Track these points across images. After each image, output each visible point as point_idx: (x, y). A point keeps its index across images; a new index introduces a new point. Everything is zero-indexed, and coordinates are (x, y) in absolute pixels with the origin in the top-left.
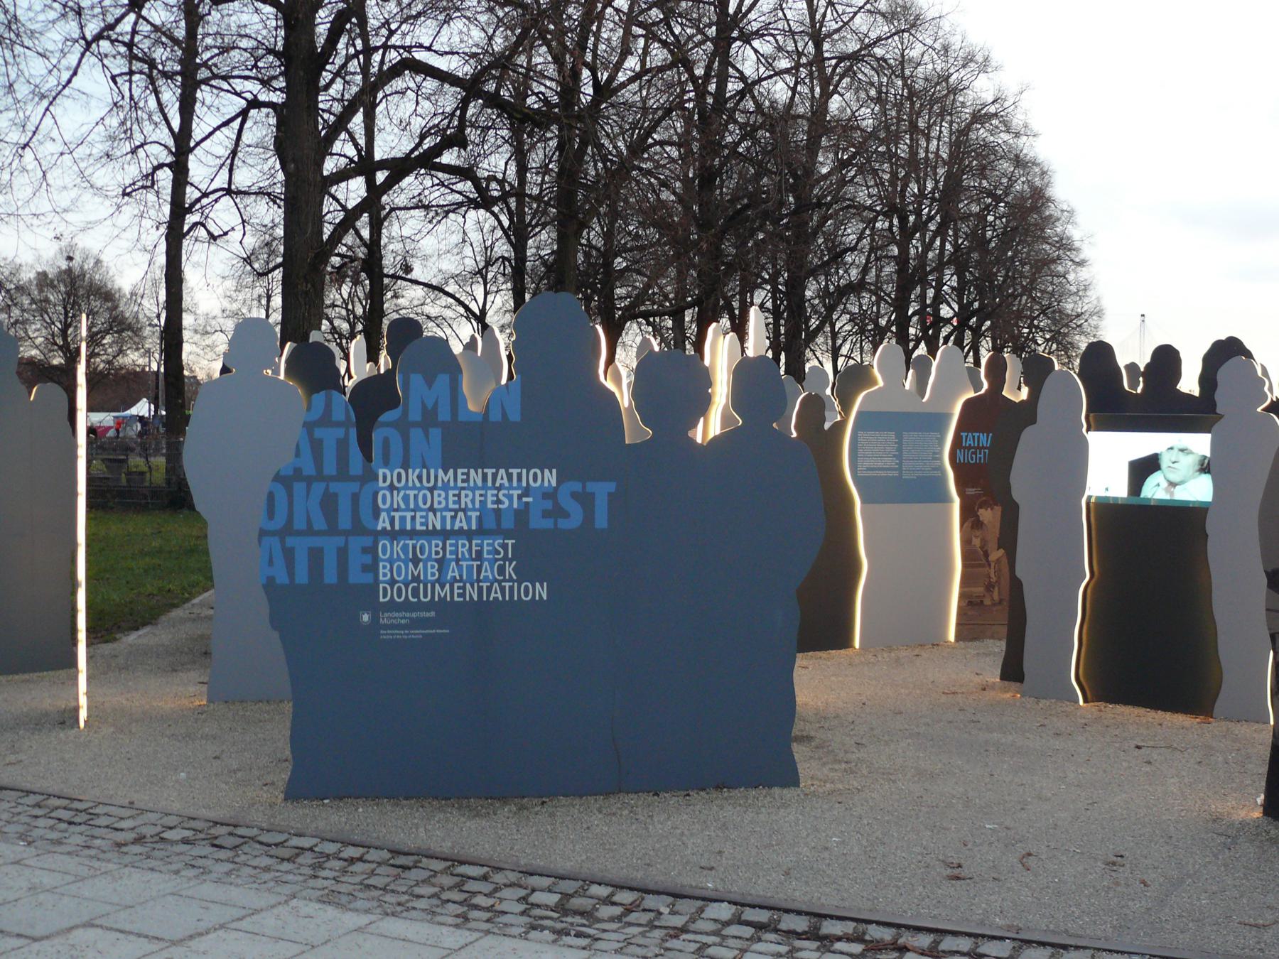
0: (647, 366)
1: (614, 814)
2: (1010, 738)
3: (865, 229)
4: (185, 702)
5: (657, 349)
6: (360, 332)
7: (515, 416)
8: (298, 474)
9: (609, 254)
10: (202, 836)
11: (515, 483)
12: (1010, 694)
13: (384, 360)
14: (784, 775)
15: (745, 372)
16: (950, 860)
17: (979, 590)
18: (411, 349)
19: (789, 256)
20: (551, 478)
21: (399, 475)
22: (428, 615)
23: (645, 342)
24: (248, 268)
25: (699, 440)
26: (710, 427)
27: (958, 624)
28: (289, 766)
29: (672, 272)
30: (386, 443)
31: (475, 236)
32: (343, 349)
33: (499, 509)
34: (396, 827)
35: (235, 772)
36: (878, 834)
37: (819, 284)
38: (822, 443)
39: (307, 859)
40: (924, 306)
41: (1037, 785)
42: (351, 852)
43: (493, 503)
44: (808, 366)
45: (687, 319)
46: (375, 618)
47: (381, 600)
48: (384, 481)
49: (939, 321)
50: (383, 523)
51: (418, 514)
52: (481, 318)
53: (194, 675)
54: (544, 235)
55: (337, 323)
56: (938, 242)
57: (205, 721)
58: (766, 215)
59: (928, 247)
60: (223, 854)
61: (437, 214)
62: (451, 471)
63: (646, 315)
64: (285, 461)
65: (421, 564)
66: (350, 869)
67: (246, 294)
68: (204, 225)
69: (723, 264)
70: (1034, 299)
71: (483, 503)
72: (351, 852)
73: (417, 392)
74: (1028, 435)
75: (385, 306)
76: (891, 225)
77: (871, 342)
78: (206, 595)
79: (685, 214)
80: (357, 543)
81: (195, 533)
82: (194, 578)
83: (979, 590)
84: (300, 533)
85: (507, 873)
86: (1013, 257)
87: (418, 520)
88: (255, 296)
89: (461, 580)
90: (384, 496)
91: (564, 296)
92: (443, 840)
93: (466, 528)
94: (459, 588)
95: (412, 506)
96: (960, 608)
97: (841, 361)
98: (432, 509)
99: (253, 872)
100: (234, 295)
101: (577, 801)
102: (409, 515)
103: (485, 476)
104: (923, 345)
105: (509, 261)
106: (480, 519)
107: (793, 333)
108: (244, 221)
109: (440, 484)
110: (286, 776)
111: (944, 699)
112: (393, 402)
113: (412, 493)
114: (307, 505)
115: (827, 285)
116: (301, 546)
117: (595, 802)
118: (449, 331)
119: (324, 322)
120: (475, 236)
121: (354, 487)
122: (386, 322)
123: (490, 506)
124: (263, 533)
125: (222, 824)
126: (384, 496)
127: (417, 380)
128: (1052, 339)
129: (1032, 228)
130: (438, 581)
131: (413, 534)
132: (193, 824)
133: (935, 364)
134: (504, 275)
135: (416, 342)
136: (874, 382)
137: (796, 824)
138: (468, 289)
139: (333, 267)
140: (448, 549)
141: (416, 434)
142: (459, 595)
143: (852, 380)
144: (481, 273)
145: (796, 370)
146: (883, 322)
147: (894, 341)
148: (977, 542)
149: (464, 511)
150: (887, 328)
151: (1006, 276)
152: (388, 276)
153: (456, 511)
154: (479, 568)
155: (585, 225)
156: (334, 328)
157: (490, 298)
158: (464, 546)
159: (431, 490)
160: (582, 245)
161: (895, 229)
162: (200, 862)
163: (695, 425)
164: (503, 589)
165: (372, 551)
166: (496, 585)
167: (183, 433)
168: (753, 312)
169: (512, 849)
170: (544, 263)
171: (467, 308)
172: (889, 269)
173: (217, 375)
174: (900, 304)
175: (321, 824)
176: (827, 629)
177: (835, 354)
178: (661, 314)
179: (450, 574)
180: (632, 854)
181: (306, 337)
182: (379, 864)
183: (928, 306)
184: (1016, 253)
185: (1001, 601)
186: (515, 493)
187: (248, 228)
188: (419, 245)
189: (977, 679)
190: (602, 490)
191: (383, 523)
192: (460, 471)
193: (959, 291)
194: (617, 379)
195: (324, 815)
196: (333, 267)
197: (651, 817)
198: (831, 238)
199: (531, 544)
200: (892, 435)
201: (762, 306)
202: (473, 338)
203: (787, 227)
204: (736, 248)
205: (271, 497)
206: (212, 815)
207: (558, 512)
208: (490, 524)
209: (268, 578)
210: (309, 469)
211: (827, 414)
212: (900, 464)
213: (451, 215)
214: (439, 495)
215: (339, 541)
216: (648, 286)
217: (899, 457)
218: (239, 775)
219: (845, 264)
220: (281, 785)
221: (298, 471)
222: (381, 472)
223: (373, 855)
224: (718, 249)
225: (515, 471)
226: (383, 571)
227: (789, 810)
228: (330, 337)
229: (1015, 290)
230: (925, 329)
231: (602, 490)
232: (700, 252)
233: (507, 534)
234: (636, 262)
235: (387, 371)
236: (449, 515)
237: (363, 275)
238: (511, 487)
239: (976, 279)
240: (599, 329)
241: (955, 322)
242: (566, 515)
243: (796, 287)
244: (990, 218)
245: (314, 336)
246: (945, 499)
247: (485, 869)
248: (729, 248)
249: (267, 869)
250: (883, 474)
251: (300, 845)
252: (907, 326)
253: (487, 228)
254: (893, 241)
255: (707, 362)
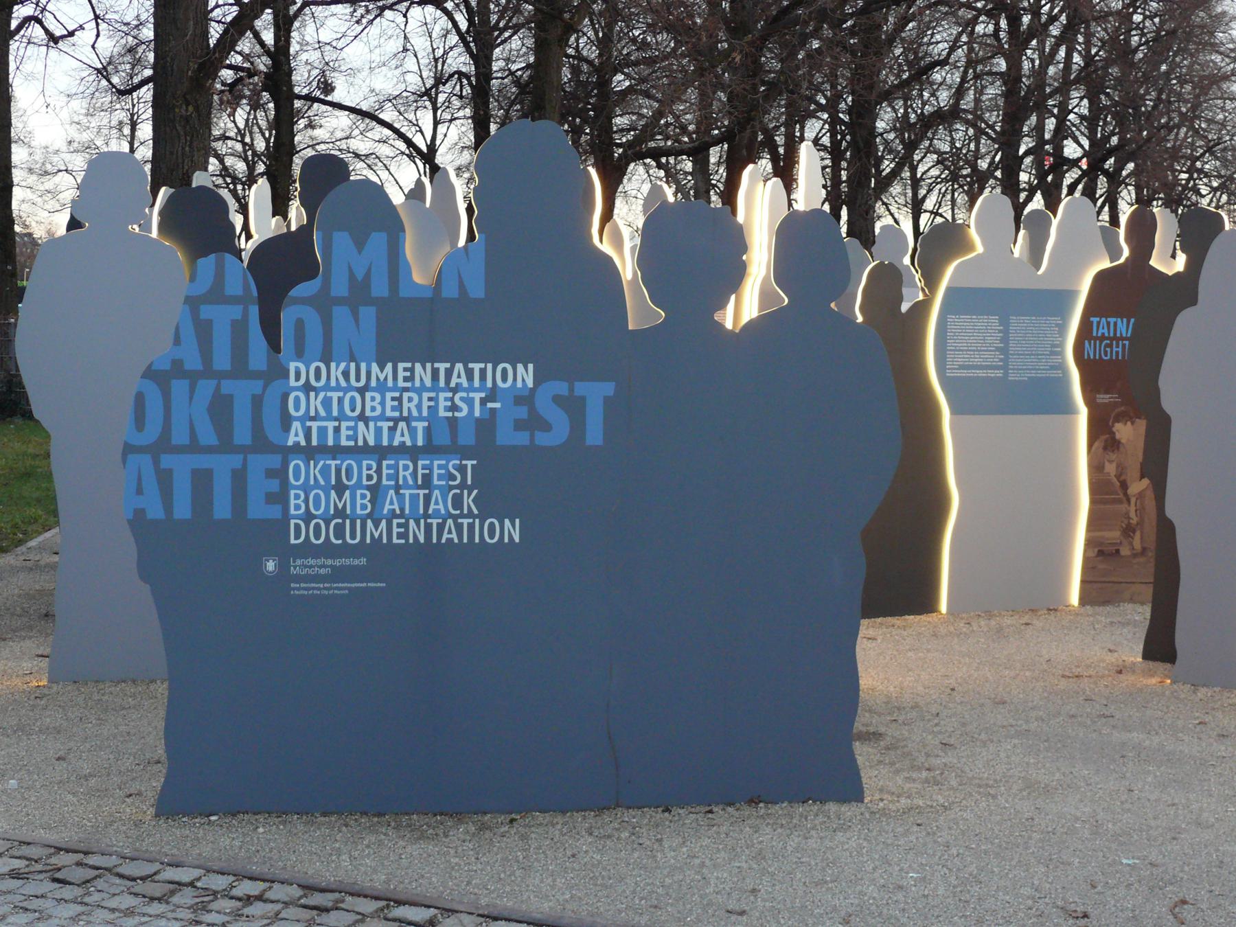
0: (658, 222)
1: (609, 837)
2: (1156, 740)
3: (960, 34)
4: (17, 682)
5: (671, 199)
6: (262, 174)
7: (477, 290)
8: (178, 369)
9: (605, 70)
10: (39, 867)
11: (477, 383)
12: (1156, 679)
13: (296, 213)
14: (845, 787)
15: (793, 232)
16: (1073, 907)
17: (1114, 535)
18: (336, 196)
19: (855, 73)
20: (525, 375)
21: (318, 370)
22: (356, 562)
23: (655, 191)
24: (104, 83)
25: (729, 325)
26: (744, 307)
27: (1084, 582)
28: (162, 769)
29: (692, 94)
30: (300, 325)
31: (420, 43)
32: (238, 199)
33: (455, 419)
34: (311, 853)
35: (86, 778)
36: (973, 868)
37: (895, 111)
38: (897, 330)
39: (185, 898)
40: (1041, 142)
41: (1195, 806)
42: (247, 888)
43: (448, 409)
44: (878, 226)
45: (713, 160)
46: (283, 566)
47: (293, 541)
48: (298, 378)
49: (1062, 163)
50: (296, 436)
51: (344, 425)
52: (429, 156)
53: (31, 645)
54: (515, 43)
55: (229, 161)
56: (1062, 53)
57: (45, 708)
58: (823, 16)
59: (1048, 60)
60: (68, 892)
61: (368, 11)
62: (389, 365)
63: (656, 154)
64: (160, 351)
65: (347, 493)
66: (246, 911)
67: (102, 119)
68: (40, 22)
69: (763, 83)
70: (1196, 132)
71: (433, 410)
72: (247, 888)
73: (341, 256)
74: (1185, 320)
75: (296, 139)
76: (997, 29)
77: (967, 193)
78: (48, 535)
79: (711, 14)
80: (259, 463)
81: (31, 451)
82: (32, 511)
83: (1114, 535)
84: (178, 450)
85: (463, 916)
86: (1167, 73)
87: (344, 433)
88: (114, 123)
89: (402, 515)
90: (297, 399)
91: (547, 127)
92: (375, 871)
93: (409, 443)
94: (399, 525)
95: (335, 413)
96: (1087, 561)
97: (924, 219)
98: (362, 417)
99: (110, 916)
100: (84, 120)
101: (559, 819)
102: (331, 425)
103: (435, 373)
104: (1038, 196)
105: (468, 77)
106: (428, 431)
107: (859, 180)
108: (97, 17)
109: (373, 383)
110: (158, 784)
111: (1063, 684)
112: (310, 270)
113: (335, 396)
114: (191, 410)
115: (906, 114)
116: (182, 467)
117: (582, 821)
118: (384, 175)
119: (212, 160)
120: (420, 43)
121: (256, 386)
122: (298, 162)
123: (442, 413)
124: (128, 449)
125: (68, 851)
126: (297, 399)
127: (342, 240)
128: (1222, 188)
129: (1197, 31)
130: (370, 516)
132: (25, 851)
133: (1055, 222)
134: (461, 97)
135: (342, 188)
136: (970, 247)
137: (860, 854)
138: (411, 117)
139: (223, 84)
140: (385, 472)
141: (341, 314)
142: (400, 536)
143: (940, 244)
144: (429, 94)
145: (862, 231)
146: (983, 165)
147: (999, 190)
148: (1111, 469)
149: (407, 420)
150: (989, 173)
151: (1158, 100)
152: (299, 97)
153: (396, 421)
154: (427, 499)
155: (572, 28)
156: (225, 168)
157: (442, 129)
158: (406, 468)
159: (362, 391)
160: (568, 56)
161: (1002, 34)
162: (35, 904)
163: (722, 305)
164: (459, 528)
165: (280, 474)
166: (450, 521)
167: (16, 312)
168: (806, 152)
169: (469, 883)
170: (517, 82)
171: (409, 143)
172: (993, 90)
173: (62, 231)
174: (1008, 140)
175: (206, 850)
176: (900, 584)
177: (917, 208)
178: (677, 153)
179: (387, 507)
180: (634, 892)
181: (188, 182)
182: (286, 904)
183: (1047, 142)
184: (1173, 66)
185: (1144, 550)
186: (477, 396)
187: (103, 26)
188: (343, 54)
189: (1111, 658)
190: (596, 393)
191: (296, 436)
192: (401, 366)
193: (1091, 121)
194: (618, 241)
195: (210, 837)
196: (223, 84)
197: (660, 841)
198: (914, 47)
199: (496, 463)
200: (994, 320)
201: (816, 141)
202: (419, 183)
203: (852, 32)
204: (782, 61)
205: (140, 399)
206: (53, 838)
207: (534, 423)
208: (443, 439)
209: (136, 511)
210: (193, 362)
211: (905, 291)
212: (1005, 361)
213: (387, 13)
214: (373, 399)
215: (236, 461)
216: (659, 114)
217: (1004, 351)
218: (93, 782)
219: (932, 84)
220: (151, 795)
221: (177, 364)
222: (292, 366)
223: (278, 892)
224: (756, 61)
225: (477, 367)
226: (295, 502)
227: (848, 834)
228: (220, 181)
229: (1170, 119)
230: (1041, 176)
231: (596, 393)
232: (731, 67)
233: (465, 453)
234: (643, 80)
235: (301, 228)
236: (386, 425)
237: (266, 95)
238: (471, 389)
239: (1116, 104)
240: (592, 171)
241: (1084, 164)
242: (546, 427)
243: (863, 114)
244: (1137, 18)
245: (199, 179)
246: (1068, 409)
247: (432, 911)
248: (771, 62)
249: (129, 912)
250: (981, 373)
251: (177, 879)
252: (1018, 167)
253: (437, 31)
254: (999, 51)
255: (740, 218)
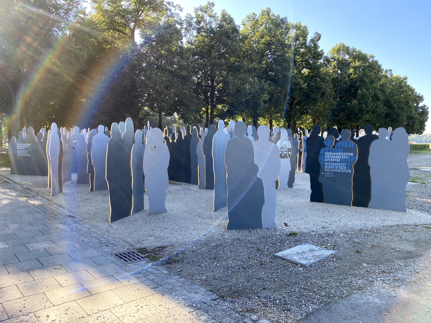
46: (324, 174)
50: (326, 160)
131: (330, 162)
